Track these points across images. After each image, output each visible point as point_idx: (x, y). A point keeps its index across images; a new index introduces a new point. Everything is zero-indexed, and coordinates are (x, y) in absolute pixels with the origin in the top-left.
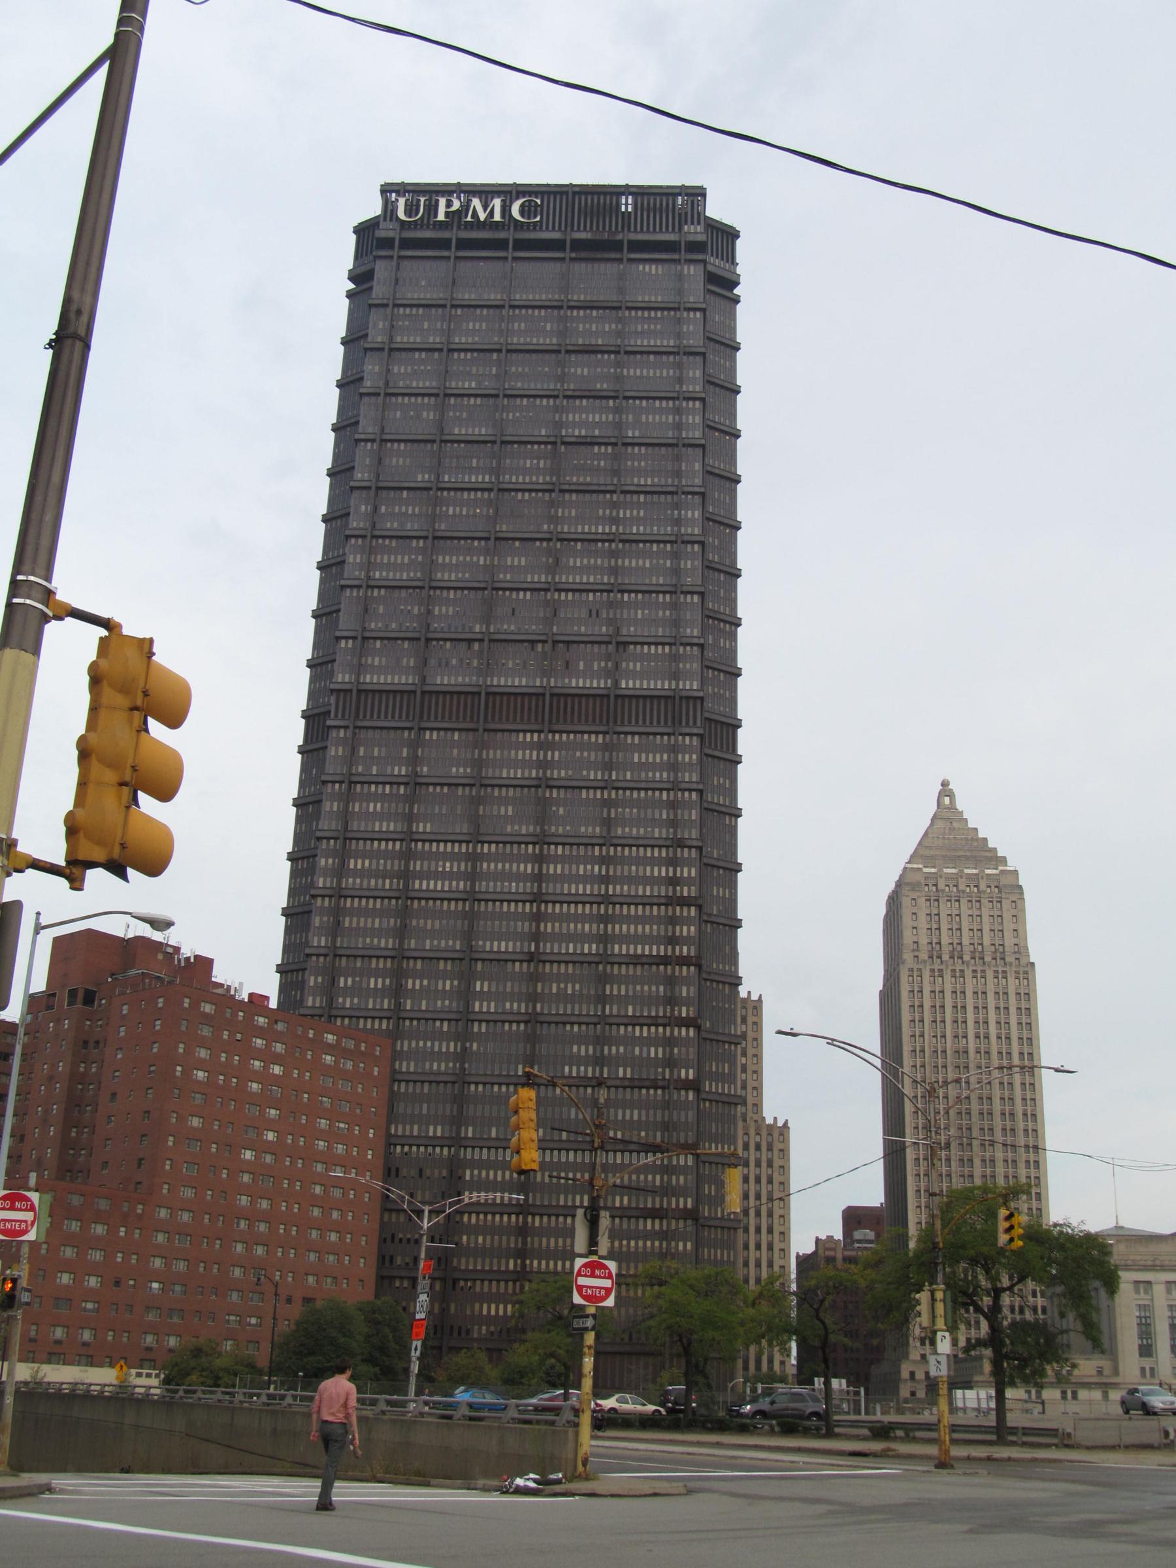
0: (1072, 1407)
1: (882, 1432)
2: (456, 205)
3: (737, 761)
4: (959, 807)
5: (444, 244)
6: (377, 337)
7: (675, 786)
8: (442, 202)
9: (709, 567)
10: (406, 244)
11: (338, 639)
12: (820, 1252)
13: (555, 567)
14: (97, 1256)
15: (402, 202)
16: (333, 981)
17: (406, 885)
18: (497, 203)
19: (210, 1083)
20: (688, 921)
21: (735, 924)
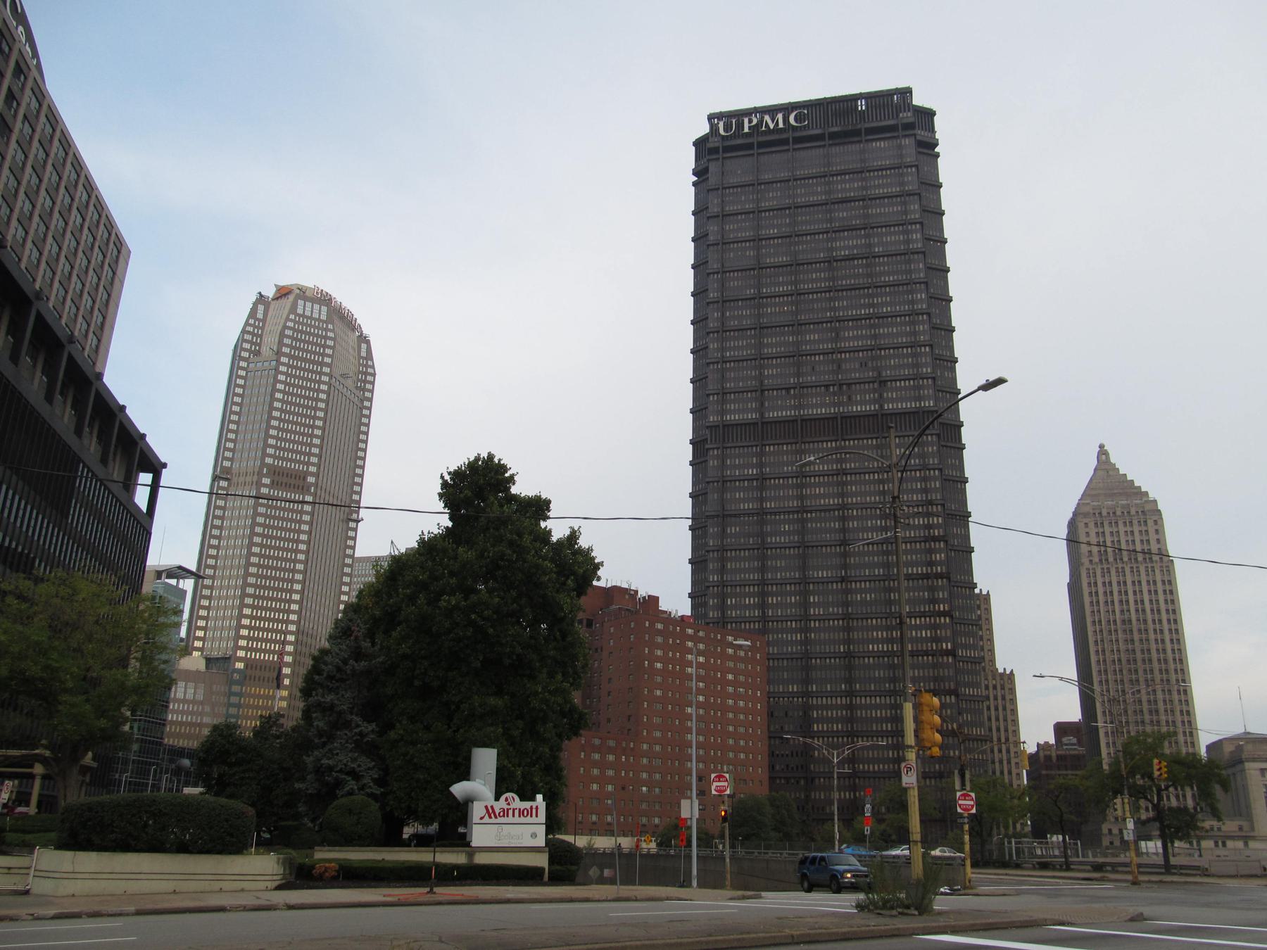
0: (1221, 851)
1: (1098, 868)
2: (755, 121)
3: (963, 447)
4: (1113, 461)
5: (749, 146)
6: (714, 209)
7: (925, 467)
8: (746, 120)
9: (934, 328)
10: (727, 149)
11: (708, 395)
12: (1041, 754)
13: (837, 338)
14: (610, 773)
15: (721, 125)
16: (724, 602)
17: (763, 541)
18: (780, 116)
19: (665, 669)
20: (940, 551)
21: (971, 550)
